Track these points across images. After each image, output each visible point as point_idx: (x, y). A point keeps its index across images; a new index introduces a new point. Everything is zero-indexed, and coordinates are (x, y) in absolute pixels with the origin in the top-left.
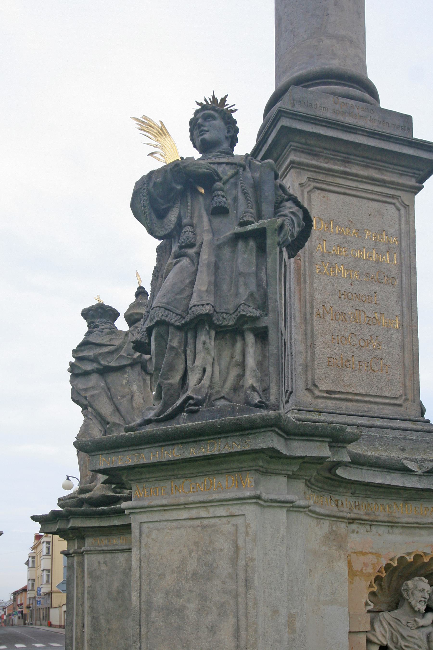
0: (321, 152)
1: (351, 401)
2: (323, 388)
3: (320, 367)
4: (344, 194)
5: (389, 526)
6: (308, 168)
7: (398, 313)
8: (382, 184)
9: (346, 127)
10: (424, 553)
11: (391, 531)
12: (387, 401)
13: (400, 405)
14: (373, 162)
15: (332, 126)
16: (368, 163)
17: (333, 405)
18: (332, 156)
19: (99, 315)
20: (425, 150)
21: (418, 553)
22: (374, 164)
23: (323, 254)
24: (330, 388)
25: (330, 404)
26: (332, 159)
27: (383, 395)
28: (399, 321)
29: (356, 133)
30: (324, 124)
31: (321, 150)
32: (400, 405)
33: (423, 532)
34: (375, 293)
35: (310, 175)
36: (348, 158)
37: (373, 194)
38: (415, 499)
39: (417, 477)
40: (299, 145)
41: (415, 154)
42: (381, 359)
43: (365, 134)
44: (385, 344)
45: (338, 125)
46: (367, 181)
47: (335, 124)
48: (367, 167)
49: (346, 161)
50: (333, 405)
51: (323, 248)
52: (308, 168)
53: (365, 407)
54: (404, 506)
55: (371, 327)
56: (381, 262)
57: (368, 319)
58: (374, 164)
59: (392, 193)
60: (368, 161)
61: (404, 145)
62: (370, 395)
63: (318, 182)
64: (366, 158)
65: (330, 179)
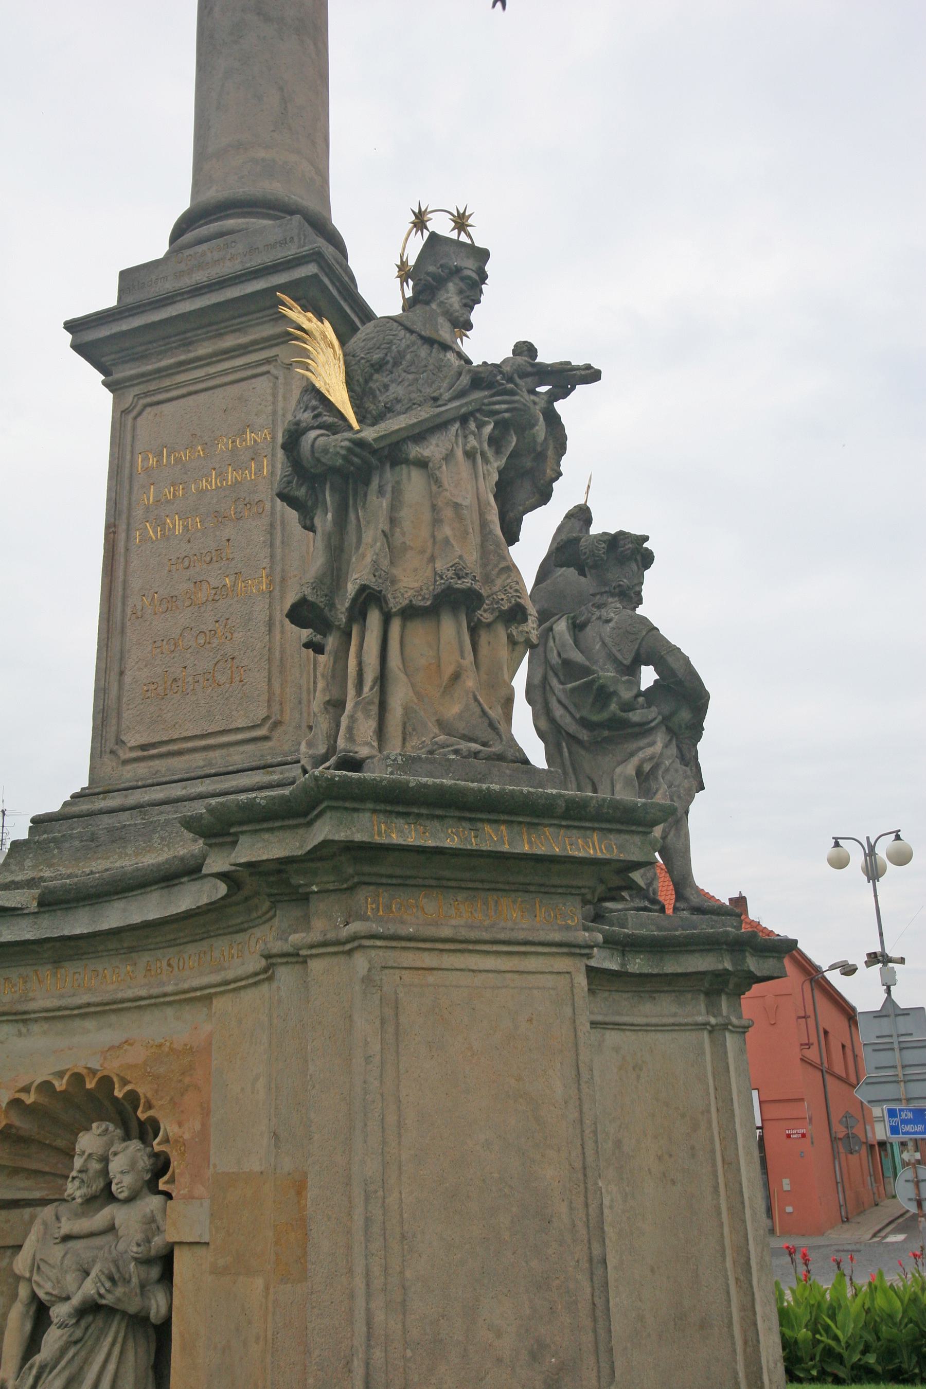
0: (146, 350)
1: (180, 753)
2: (132, 743)
3: (130, 707)
4: (190, 394)
5: (17, 1021)
6: (131, 383)
7: (266, 562)
8: (242, 351)
9: (158, 301)
10: (89, 1068)
11: (24, 1030)
12: (240, 736)
13: (266, 738)
14: (223, 325)
15: (139, 310)
16: (217, 330)
17: (147, 770)
18: (163, 348)
19: (646, 539)
20: (283, 270)
21: (76, 1070)
22: (226, 327)
23: (147, 509)
24: (143, 740)
25: (142, 770)
26: (166, 351)
27: (233, 726)
28: (267, 577)
29: (175, 302)
30: (127, 314)
31: (143, 348)
32: (266, 738)
33: (89, 1024)
34: (228, 540)
35: (136, 390)
36: (186, 338)
37: (236, 371)
38: (70, 958)
39: (31, 917)
40: (113, 356)
41: (208, 303)
42: (233, 659)
43: (185, 297)
44: (240, 629)
45: (144, 305)
46: (219, 358)
47: (139, 306)
48: (220, 335)
49: (187, 344)
50: (147, 770)
51: (148, 499)
52: (131, 383)
53: (178, 764)
54: (55, 974)
55: (217, 604)
56: (240, 483)
57: (213, 592)
58: (226, 327)
59: (263, 357)
60: (215, 327)
61: (249, 280)
62: (209, 734)
63: (153, 395)
64: (210, 324)
65: (167, 382)
